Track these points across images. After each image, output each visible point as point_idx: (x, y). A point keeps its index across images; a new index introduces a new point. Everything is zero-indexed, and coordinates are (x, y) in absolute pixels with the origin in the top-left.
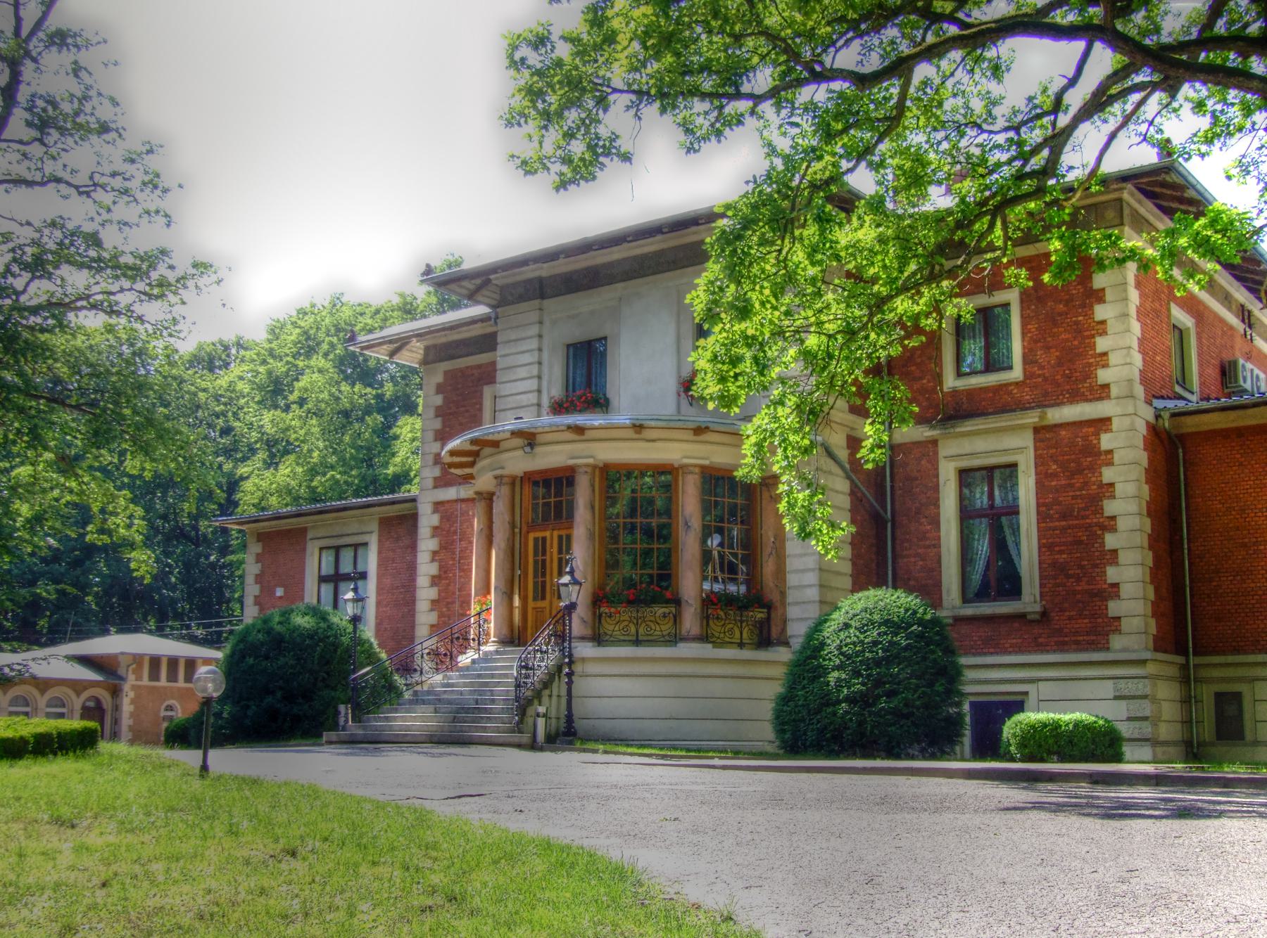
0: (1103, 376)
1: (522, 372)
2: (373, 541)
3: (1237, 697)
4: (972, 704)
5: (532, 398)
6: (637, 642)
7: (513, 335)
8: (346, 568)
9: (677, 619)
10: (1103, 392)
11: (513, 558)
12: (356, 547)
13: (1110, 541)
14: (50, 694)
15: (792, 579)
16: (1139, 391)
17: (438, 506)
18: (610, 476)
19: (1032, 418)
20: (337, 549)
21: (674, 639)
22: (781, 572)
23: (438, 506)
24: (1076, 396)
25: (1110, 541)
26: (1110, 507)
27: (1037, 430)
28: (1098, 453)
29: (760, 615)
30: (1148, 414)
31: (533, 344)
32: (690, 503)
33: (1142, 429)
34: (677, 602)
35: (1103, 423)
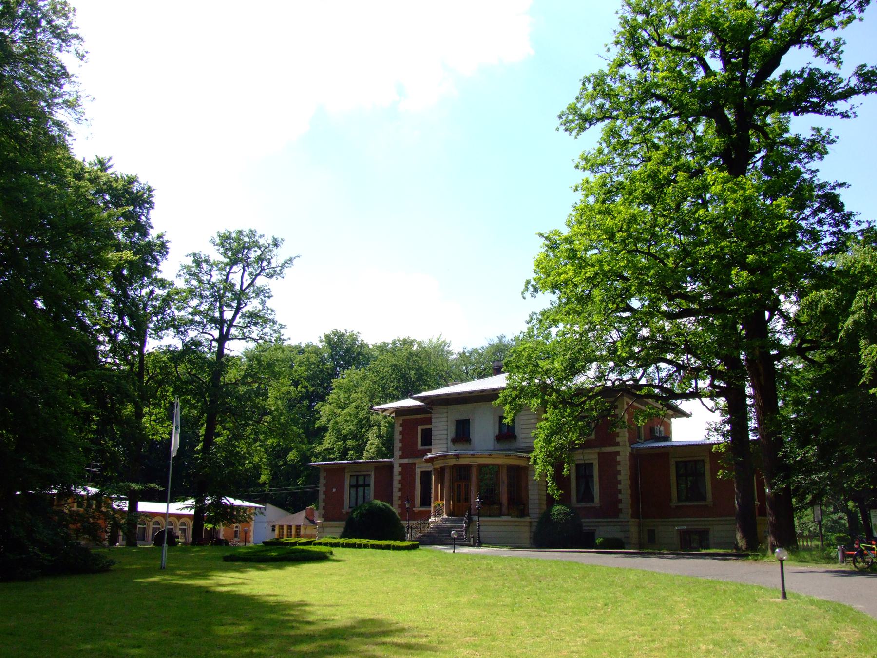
0: (618, 439)
1: (441, 428)
2: (373, 474)
3: (653, 531)
4: (376, 497)
5: (445, 437)
6: (490, 516)
7: (437, 416)
8: (361, 482)
9: (501, 509)
10: (617, 444)
11: (451, 489)
12: (365, 476)
13: (620, 487)
14: (182, 520)
15: (530, 497)
16: (627, 444)
17: (401, 465)
18: (481, 467)
19: (597, 450)
20: (357, 476)
21: (500, 515)
22: (527, 495)
23: (401, 465)
24: (610, 445)
25: (620, 487)
26: (620, 477)
27: (599, 454)
28: (616, 461)
29: (522, 507)
30: (629, 450)
31: (445, 419)
32: (504, 477)
33: (628, 454)
34: (501, 504)
35: (618, 453)
